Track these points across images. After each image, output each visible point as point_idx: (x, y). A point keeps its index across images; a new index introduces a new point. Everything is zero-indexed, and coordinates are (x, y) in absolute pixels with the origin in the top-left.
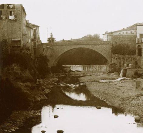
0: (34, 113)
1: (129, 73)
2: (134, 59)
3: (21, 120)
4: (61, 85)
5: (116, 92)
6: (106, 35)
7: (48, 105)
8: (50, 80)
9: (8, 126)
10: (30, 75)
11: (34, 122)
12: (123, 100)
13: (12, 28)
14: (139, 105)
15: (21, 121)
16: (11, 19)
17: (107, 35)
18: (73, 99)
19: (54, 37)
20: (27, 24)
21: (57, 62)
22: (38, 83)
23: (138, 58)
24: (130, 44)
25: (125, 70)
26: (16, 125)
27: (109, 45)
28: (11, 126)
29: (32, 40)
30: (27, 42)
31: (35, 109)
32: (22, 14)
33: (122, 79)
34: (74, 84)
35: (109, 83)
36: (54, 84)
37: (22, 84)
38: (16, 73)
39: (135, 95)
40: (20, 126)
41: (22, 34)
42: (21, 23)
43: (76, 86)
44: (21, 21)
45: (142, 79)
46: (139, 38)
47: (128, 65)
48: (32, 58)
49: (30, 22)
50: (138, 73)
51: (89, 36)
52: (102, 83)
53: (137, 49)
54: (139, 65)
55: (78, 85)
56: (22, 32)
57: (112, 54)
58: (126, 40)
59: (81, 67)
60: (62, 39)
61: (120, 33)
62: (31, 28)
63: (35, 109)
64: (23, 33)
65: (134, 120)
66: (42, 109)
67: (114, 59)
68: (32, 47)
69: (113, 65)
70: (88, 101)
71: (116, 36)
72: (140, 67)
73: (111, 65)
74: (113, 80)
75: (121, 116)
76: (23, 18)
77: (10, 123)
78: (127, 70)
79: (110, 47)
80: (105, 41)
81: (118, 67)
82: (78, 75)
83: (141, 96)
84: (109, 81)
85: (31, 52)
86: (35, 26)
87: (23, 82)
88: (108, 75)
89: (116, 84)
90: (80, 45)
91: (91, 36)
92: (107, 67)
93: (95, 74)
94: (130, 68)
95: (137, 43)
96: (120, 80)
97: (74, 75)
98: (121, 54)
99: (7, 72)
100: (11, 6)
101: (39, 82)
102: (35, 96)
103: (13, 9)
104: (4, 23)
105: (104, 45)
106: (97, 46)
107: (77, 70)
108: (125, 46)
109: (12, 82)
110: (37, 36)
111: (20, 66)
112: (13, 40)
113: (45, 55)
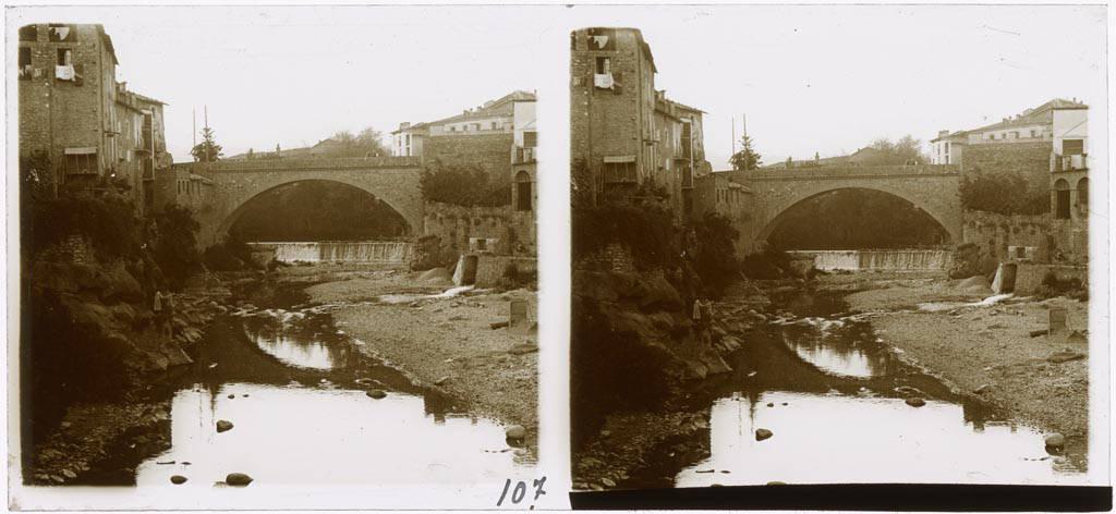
0: (147, 412)
1: (485, 269)
2: (504, 219)
3: (99, 439)
4: (243, 312)
5: (439, 339)
6: (403, 135)
7: (196, 386)
8: (202, 296)
9: (52, 461)
10: (669, 285)
11: (145, 444)
12: (465, 365)
13: (66, 109)
14: (521, 383)
15: (98, 442)
16: (64, 78)
17: (408, 136)
18: (284, 365)
19: (217, 141)
20: (660, 102)
21: (229, 232)
22: (158, 307)
23: (1057, 224)
24: (488, 167)
25: (1012, 269)
26: (79, 455)
27: (414, 171)
28: (602, 470)
29: (138, 153)
30: (121, 160)
31: (148, 398)
32: (104, 60)
33: (461, 293)
34: (830, 319)
35: (415, 306)
36: (217, 310)
37: (640, 317)
38: (618, 280)
39: (508, 349)
40: (94, 459)
41: (100, 131)
42: (99, 93)
43: (295, 316)
44: (635, 94)
45: (1070, 301)
46: (521, 144)
47: (481, 244)
48: (137, 216)
49: (128, 88)
50: (1058, 278)
51: (341, 140)
52: (930, 313)
53: (513, 185)
54: (520, 242)
55: (301, 315)
56: (641, 131)
57: (424, 203)
58: (476, 152)
59: (313, 249)
60: (245, 151)
61: (453, 129)
62: (134, 110)
63: (148, 398)
64: (645, 138)
65: (505, 437)
66: (174, 398)
67: (432, 222)
68: (675, 186)
69: (968, 250)
70: (878, 378)
71: (440, 137)
72: (1066, 255)
73: (959, 248)
74: (969, 304)
75: (456, 426)
76: (108, 76)
77: (59, 449)
78: (480, 259)
79: (419, 177)
80: (939, 166)
81: (445, 249)
82: (304, 279)
83: (531, 352)
84: (951, 307)
85: (135, 195)
86: (147, 102)
87: (107, 302)
88: (411, 278)
89: (440, 310)
90: (851, 178)
91: (351, 138)
92: (945, 256)
93: (365, 274)
94: (488, 254)
95: (1053, 173)
96: (452, 295)
97: (287, 279)
98: (995, 212)
99: (46, 265)
100: (64, 32)
101: (163, 302)
102: (149, 354)
103: (69, 44)
104: (38, 91)
105: (396, 171)
106: (371, 175)
107: (839, 268)
108: (472, 173)
109: (604, 310)
110: (157, 139)
111: (633, 254)
112: (68, 151)
113: (183, 205)
